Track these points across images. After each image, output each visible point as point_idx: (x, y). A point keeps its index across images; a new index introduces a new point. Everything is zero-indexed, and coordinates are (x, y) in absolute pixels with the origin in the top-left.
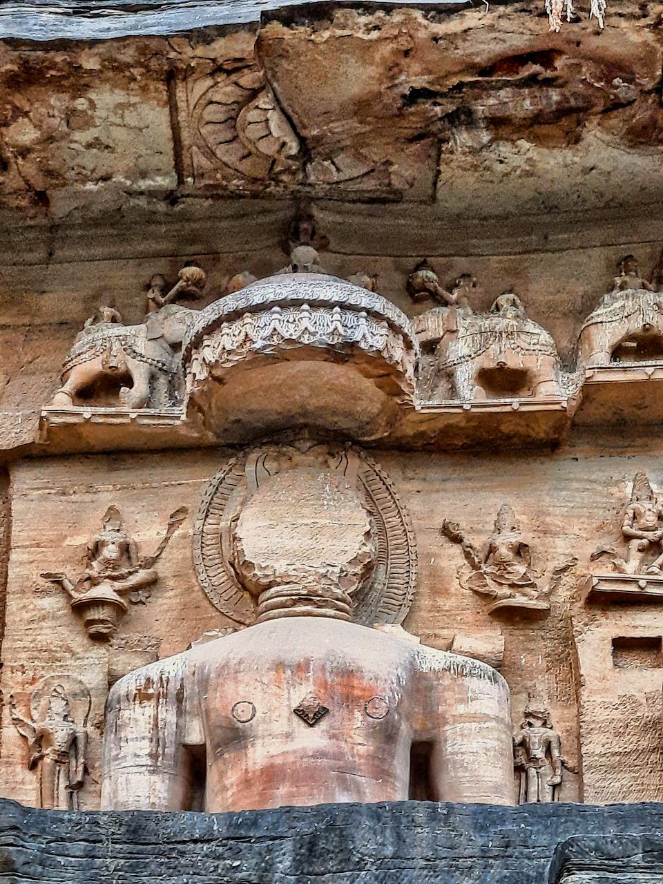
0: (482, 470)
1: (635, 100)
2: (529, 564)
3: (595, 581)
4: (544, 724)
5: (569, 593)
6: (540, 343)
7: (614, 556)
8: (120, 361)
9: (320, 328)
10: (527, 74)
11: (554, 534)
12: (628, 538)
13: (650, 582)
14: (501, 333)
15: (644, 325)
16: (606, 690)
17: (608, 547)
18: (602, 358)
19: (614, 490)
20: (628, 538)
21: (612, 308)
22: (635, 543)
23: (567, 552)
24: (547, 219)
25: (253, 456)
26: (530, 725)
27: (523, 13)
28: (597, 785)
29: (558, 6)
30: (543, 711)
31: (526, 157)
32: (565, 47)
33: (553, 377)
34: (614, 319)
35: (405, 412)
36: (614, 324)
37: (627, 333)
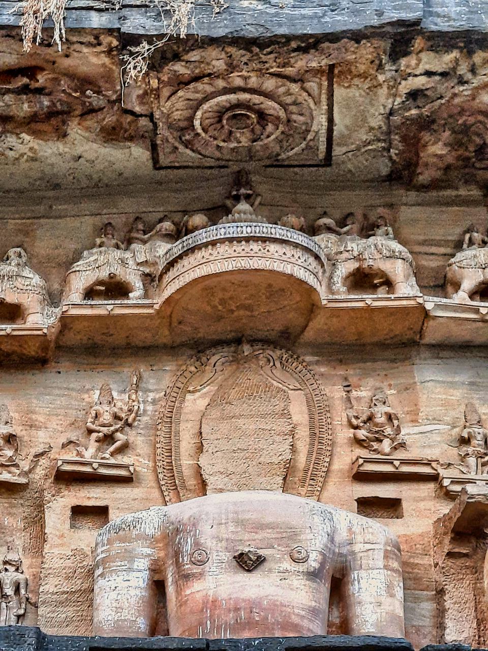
1: (104, 107)
2: (16, 450)
3: (60, 463)
4: (17, 570)
5: (44, 472)
6: (32, 284)
7: (78, 445)
10: (20, 84)
11: (38, 428)
12: (90, 432)
13: (101, 465)
14: (4, 276)
15: (110, 274)
16: (62, 545)
17: (75, 438)
19: (86, 396)
20: (90, 432)
21: (88, 261)
22: (94, 435)
23: (46, 441)
24: (51, 194)
26: (6, 570)
27: (7, 38)
28: (48, 616)
29: (30, 34)
30: (16, 560)
31: (28, 146)
32: (45, 65)
33: (39, 310)
34: (88, 269)
36: (88, 272)
37: (97, 279)
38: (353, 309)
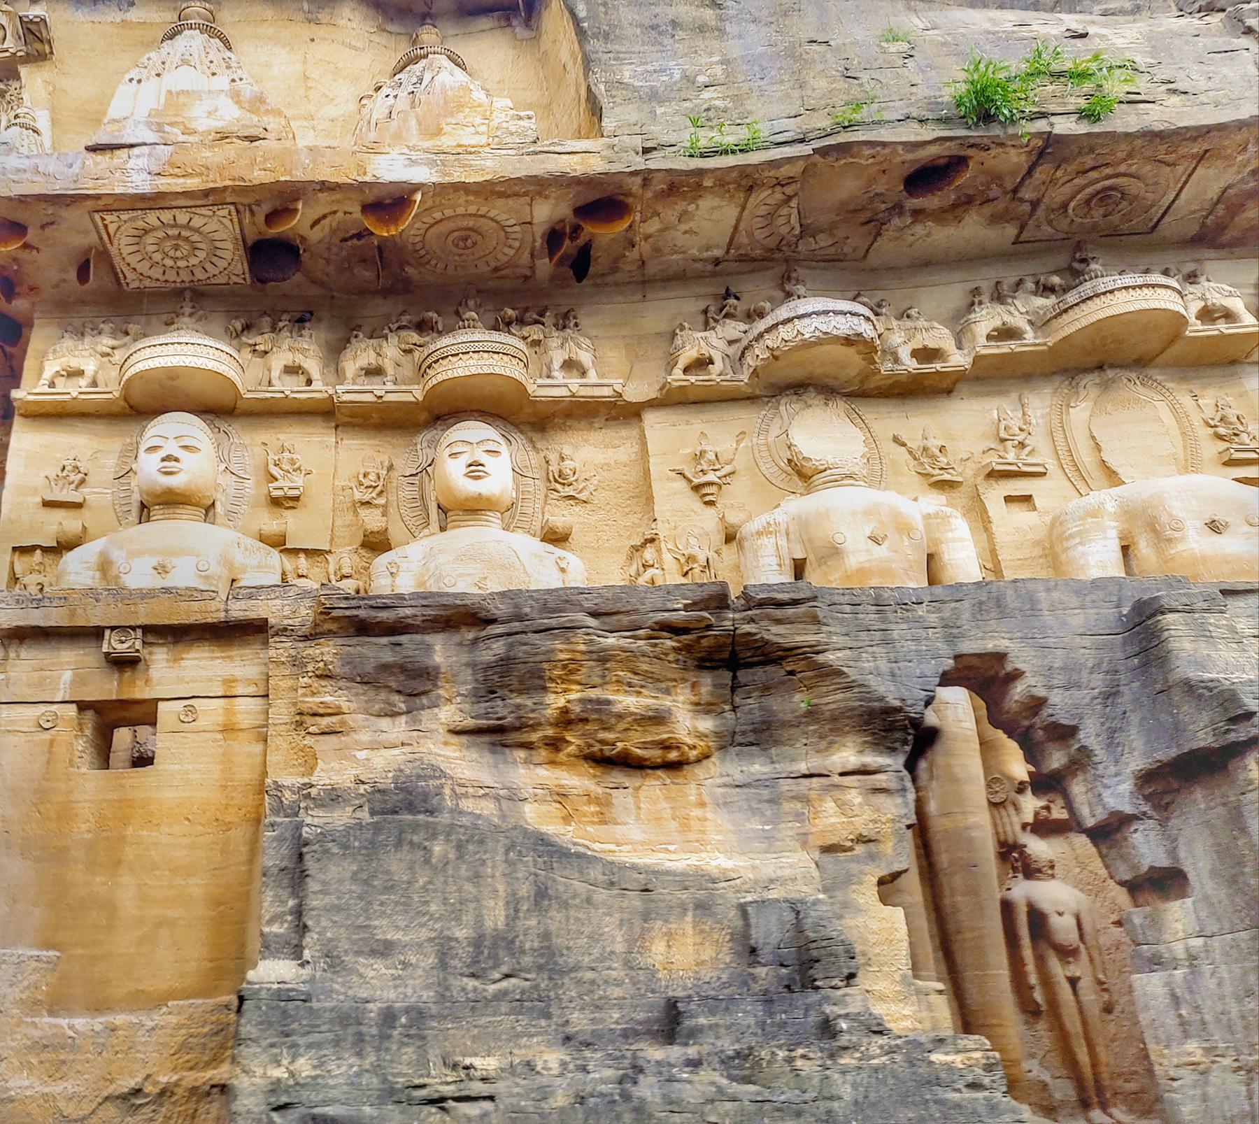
0: (911, 405)
8: (706, 351)
9: (842, 326)
18: (982, 340)
20: (1003, 440)
25: (783, 401)
35: (874, 374)
38: (1208, 337)
